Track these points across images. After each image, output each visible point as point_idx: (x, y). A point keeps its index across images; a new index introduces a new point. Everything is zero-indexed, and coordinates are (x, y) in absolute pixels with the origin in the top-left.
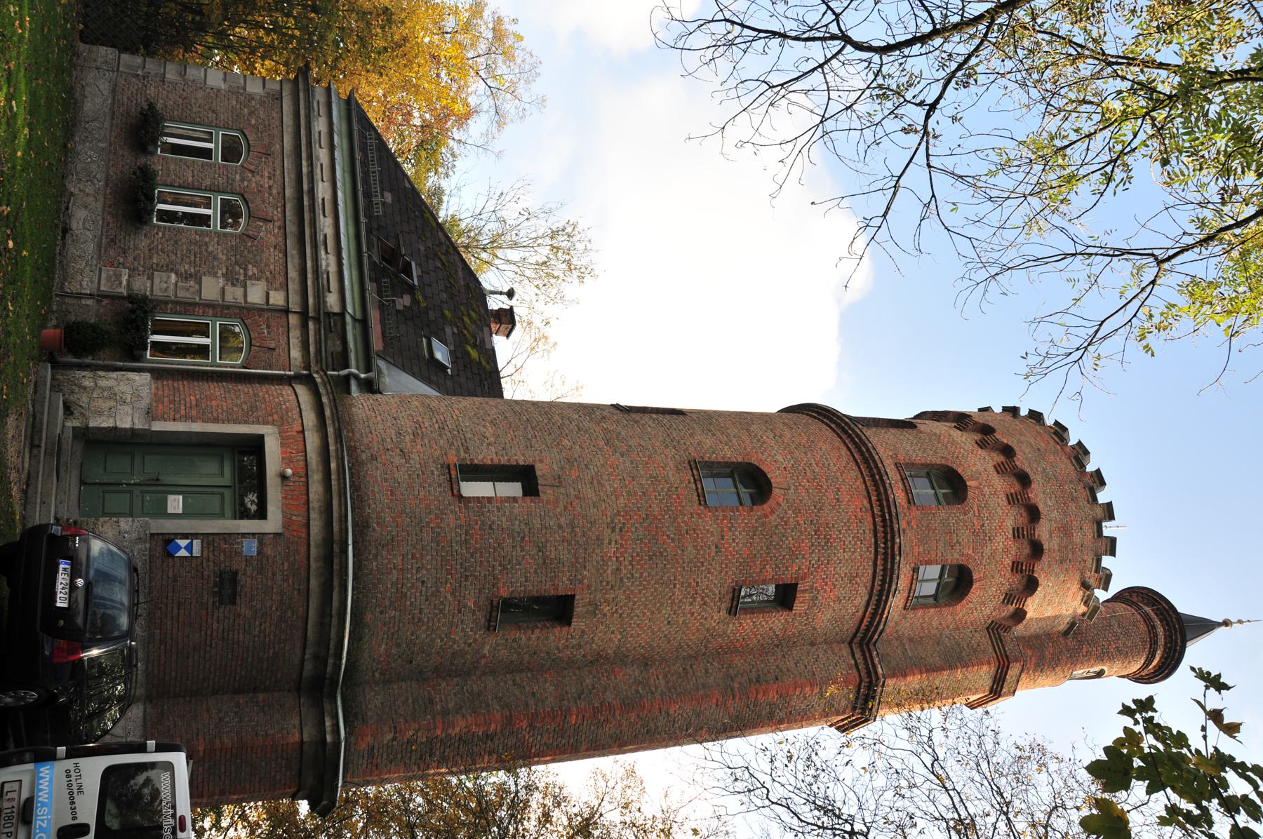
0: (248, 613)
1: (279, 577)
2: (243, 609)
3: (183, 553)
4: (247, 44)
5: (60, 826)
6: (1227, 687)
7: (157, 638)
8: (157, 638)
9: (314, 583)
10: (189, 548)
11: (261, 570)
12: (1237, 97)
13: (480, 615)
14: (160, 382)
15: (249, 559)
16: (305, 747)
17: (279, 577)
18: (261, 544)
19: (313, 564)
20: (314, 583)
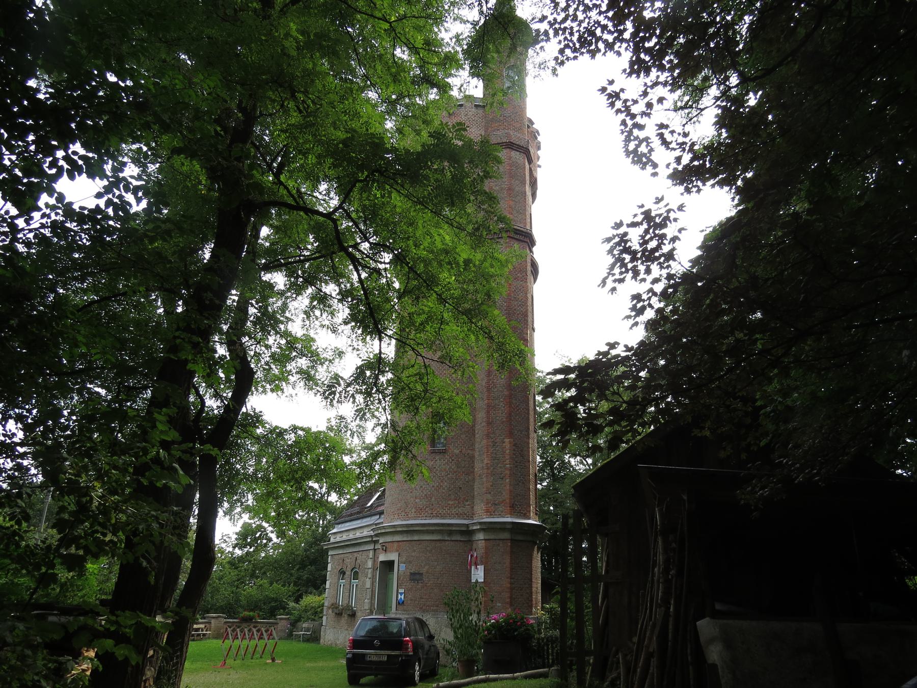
0: (427, 567)
1: (413, 554)
2: (424, 570)
3: (403, 597)
4: (54, 437)
5: (66, 194)
6: (603, 243)
7: (435, 608)
8: (435, 608)
9: (416, 538)
10: (401, 594)
11: (410, 562)
12: (437, 417)
13: (437, 458)
14: (441, 671)
15: (407, 568)
16: (487, 537)
17: (413, 554)
18: (402, 563)
19: (409, 539)
20: (416, 538)
